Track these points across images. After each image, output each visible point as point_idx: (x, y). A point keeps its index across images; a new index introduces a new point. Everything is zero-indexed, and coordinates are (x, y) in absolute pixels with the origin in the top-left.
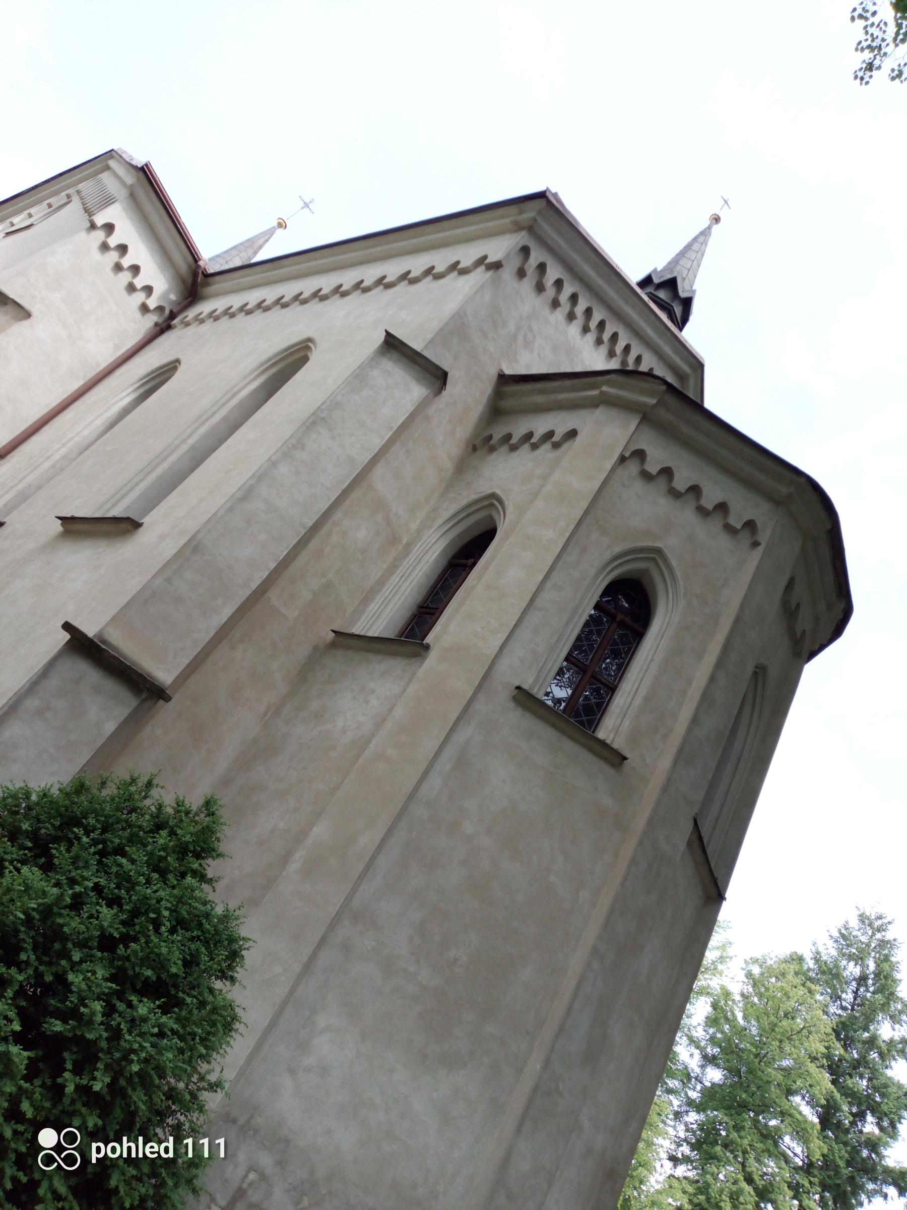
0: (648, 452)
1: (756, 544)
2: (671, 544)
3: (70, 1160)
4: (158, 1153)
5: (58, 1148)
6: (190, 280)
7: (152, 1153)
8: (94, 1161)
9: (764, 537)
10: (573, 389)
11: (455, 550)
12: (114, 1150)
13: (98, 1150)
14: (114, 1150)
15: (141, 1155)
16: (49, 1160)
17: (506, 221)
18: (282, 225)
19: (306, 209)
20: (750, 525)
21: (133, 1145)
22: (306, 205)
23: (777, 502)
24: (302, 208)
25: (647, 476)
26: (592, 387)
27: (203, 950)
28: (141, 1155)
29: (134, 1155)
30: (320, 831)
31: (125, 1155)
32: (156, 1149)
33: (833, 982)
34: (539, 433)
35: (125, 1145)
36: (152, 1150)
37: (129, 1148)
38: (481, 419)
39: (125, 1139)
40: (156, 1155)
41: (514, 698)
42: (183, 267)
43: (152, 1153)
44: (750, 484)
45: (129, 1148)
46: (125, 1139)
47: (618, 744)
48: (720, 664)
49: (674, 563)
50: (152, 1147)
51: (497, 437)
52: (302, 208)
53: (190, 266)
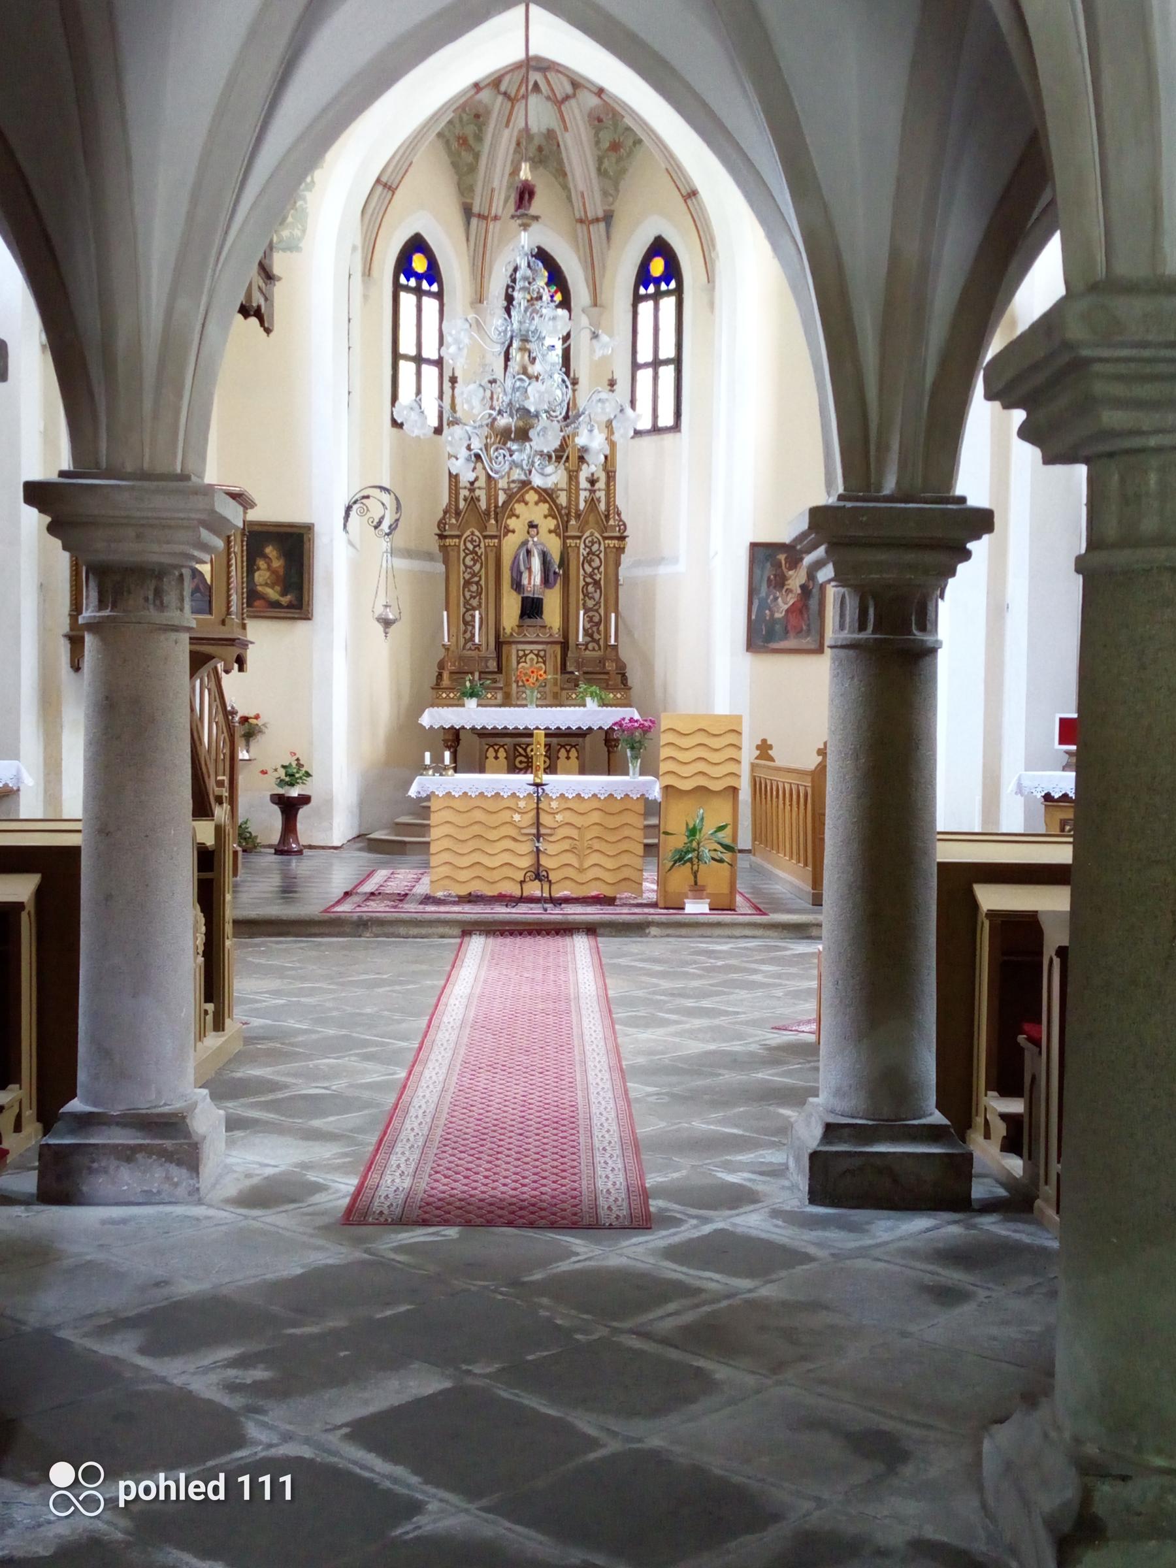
4: (205, 1494)
7: (197, 1494)
8: (122, 1505)
12: (147, 1491)
14: (147, 1491)
15: (182, 1497)
28: (182, 1497)
29: (173, 1497)
31: (162, 1497)
32: (202, 1489)
36: (197, 1490)
37: (167, 1488)
40: (202, 1497)
43: (197, 1494)
45: (167, 1488)
50: (197, 1487)
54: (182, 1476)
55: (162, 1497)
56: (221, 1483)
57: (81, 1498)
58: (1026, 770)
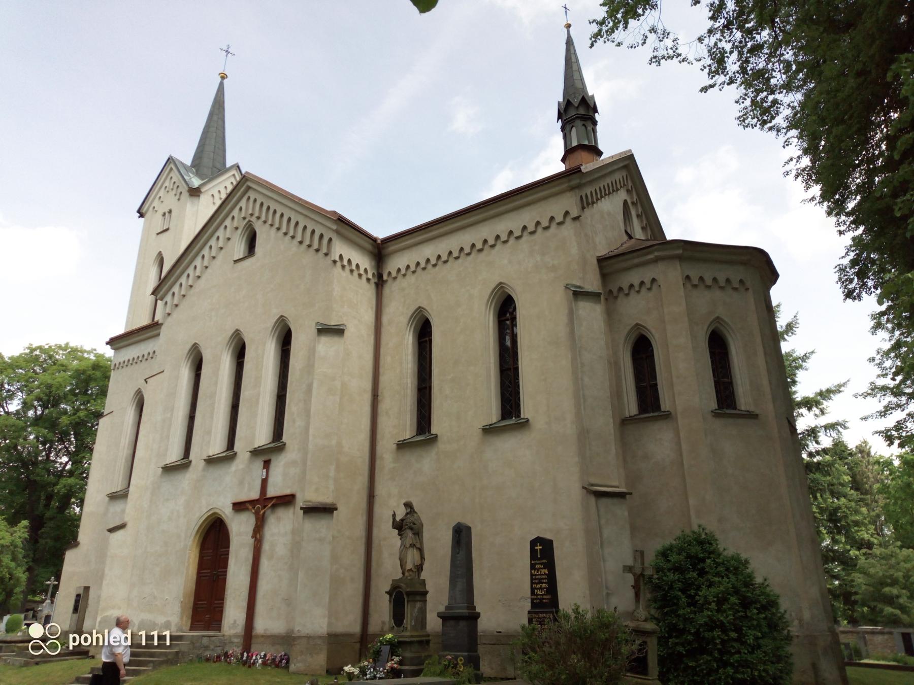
0: (690, 275)
1: (747, 289)
2: (721, 312)
3: (53, 647)
4: (120, 641)
5: (44, 639)
6: (376, 251)
7: (114, 642)
8: (71, 648)
9: (748, 283)
10: (638, 257)
11: (497, 316)
12: (86, 640)
13: (74, 640)
14: (86, 640)
15: (106, 644)
16: (37, 648)
17: (565, 186)
18: (223, 77)
19: (229, 55)
20: (741, 281)
21: (100, 636)
22: (227, 52)
23: (743, 263)
24: (227, 56)
25: (695, 286)
26: (648, 254)
27: (818, 515)
28: (106, 644)
29: (101, 644)
30: (692, 502)
31: (94, 644)
32: (118, 639)
33: (41, 461)
34: (636, 284)
35: (95, 636)
36: (115, 640)
37: (98, 638)
38: (600, 282)
40: (118, 644)
41: (713, 416)
42: (368, 246)
44: (731, 263)
45: (98, 638)
47: (752, 408)
48: (765, 353)
49: (726, 319)
51: (615, 291)
52: (227, 56)
53: (372, 245)
55: (94, 644)
56: (71, 644)
57: (47, 644)
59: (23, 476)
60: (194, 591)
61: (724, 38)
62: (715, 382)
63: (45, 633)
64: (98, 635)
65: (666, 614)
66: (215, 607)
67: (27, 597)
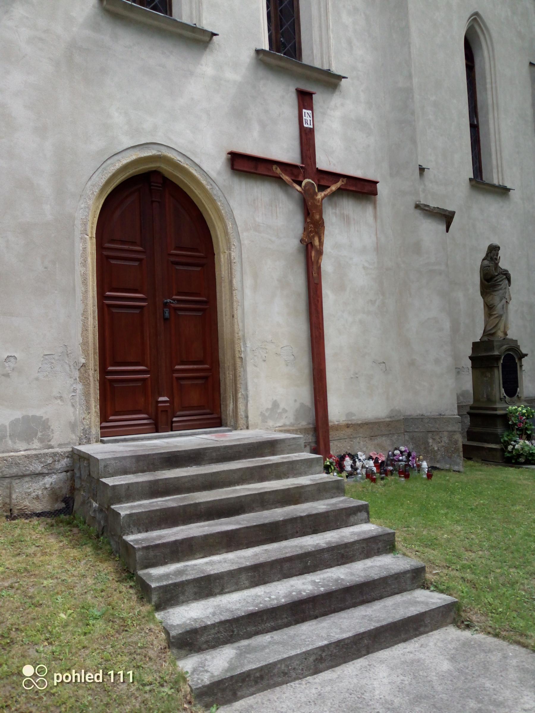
4: (93, 679)
5: (35, 676)
7: (89, 679)
12: (67, 677)
14: (67, 677)
15: (83, 681)
21: (78, 675)
28: (83, 681)
31: (74, 681)
32: (92, 677)
35: (74, 675)
36: (90, 678)
37: (76, 677)
39: (74, 671)
40: (92, 681)
43: (89, 679)
45: (76, 677)
46: (74, 671)
50: (90, 676)
54: (83, 671)
57: (33, 686)
58: (394, 534)
59: (511, 537)
60: (473, 52)
61: (299, 666)
62: (296, 624)
63: (35, 673)
64: (77, 674)
65: (72, 589)
66: (178, 379)
67: (504, 455)
